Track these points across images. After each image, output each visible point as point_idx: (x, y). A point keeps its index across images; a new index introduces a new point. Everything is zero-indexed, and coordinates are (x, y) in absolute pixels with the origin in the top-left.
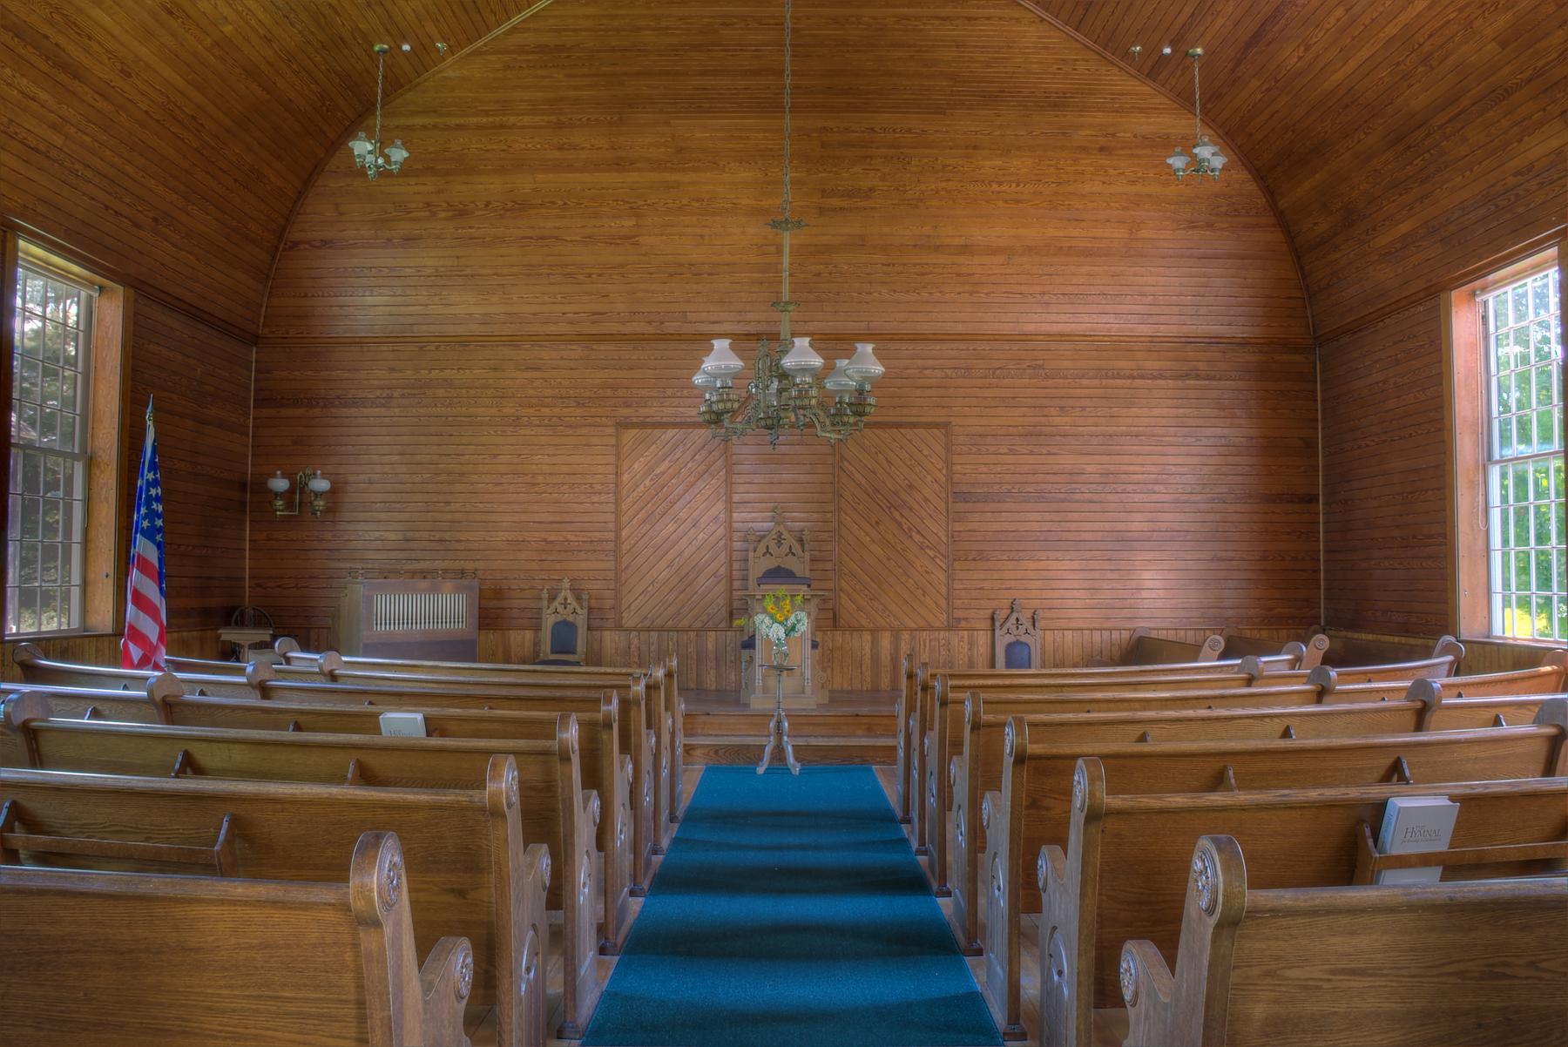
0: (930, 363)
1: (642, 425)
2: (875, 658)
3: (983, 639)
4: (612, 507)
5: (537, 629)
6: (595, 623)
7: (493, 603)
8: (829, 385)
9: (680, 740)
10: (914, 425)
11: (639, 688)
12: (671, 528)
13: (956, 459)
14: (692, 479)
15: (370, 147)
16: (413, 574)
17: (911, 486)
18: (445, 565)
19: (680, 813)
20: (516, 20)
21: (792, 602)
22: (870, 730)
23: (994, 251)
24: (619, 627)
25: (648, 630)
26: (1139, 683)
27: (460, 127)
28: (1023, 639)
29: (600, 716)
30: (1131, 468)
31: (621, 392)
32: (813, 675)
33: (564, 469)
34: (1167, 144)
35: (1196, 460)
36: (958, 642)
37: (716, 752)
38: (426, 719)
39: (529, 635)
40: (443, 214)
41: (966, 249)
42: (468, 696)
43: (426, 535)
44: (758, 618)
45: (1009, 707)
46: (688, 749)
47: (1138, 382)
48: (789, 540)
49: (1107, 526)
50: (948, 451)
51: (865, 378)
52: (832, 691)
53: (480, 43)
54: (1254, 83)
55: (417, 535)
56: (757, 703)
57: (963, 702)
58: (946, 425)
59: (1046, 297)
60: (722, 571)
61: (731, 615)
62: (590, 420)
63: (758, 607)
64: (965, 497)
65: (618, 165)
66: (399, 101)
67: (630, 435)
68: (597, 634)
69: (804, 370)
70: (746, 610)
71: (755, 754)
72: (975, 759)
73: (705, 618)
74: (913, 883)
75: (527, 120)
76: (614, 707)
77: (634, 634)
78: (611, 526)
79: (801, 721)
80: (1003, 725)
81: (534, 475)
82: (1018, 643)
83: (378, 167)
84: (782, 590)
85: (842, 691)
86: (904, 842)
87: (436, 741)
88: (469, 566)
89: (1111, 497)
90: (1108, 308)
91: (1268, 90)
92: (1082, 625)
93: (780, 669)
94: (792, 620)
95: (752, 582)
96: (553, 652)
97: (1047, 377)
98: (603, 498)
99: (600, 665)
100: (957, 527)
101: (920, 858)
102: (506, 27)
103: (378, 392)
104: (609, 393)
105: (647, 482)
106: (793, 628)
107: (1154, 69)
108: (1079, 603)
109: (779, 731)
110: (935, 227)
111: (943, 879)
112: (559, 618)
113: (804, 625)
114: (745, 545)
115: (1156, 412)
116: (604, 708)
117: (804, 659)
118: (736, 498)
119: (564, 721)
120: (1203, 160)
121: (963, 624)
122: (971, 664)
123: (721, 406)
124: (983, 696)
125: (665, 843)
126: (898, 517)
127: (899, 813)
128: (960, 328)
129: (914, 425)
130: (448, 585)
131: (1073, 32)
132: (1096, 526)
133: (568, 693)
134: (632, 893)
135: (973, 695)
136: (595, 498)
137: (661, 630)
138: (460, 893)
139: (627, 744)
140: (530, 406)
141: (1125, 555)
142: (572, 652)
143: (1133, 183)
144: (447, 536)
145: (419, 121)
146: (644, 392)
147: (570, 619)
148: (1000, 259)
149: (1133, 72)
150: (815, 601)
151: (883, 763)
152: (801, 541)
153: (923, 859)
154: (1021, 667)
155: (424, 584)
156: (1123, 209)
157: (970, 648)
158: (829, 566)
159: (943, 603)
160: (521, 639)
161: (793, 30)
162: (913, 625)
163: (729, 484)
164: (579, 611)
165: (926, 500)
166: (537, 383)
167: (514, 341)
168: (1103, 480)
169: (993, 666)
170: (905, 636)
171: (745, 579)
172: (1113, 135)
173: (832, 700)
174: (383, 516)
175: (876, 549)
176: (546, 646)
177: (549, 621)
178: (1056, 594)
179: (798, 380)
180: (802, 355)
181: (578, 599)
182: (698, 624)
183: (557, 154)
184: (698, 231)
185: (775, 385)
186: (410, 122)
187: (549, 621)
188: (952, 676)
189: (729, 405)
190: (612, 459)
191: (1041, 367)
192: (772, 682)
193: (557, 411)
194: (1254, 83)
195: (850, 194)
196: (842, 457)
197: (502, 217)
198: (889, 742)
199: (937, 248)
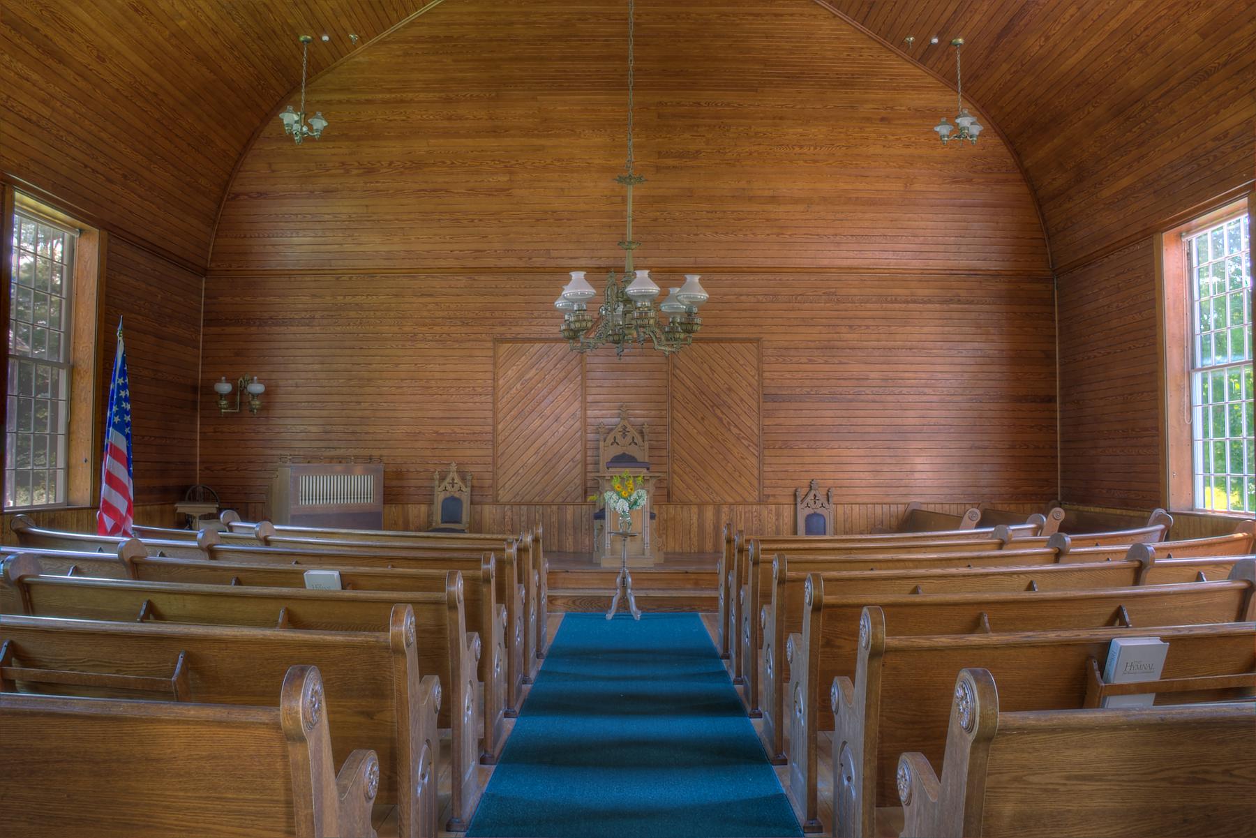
1: (514, 340)
2: (701, 527)
3: (787, 511)
5: (431, 503)
6: (477, 499)
7: (394, 483)
8: (664, 308)
9: (545, 592)
10: (732, 340)
11: (512, 551)
12: (537, 422)
13: (766, 367)
14: (554, 383)
15: (296, 118)
16: (331, 459)
17: (730, 389)
19: (545, 651)
20: (414, 16)
21: (634, 482)
22: (697, 584)
23: (796, 201)
24: (496, 502)
25: (520, 504)
27: (368, 102)
28: (819, 511)
30: (907, 375)
31: (497, 314)
32: (651, 540)
33: (452, 375)
34: (935, 115)
35: (958, 368)
36: (767, 514)
37: (574, 602)
38: (341, 575)
39: (423, 508)
40: (355, 172)
41: (773, 199)
42: (375, 557)
43: (341, 428)
44: (607, 495)
45: (807, 565)
46: (551, 599)
47: (911, 306)
48: (633, 432)
49: (887, 421)
52: (666, 554)
53: (384, 34)
55: (334, 428)
56: (607, 562)
57: (771, 562)
58: (758, 340)
60: (579, 457)
61: (586, 493)
62: (473, 337)
63: (607, 486)
64: (774, 398)
65: (495, 132)
66: (320, 81)
68: (478, 508)
69: (644, 296)
70: (598, 489)
71: (605, 603)
72: (781, 608)
74: (731, 707)
75: (422, 96)
76: (492, 566)
77: (507, 507)
78: (490, 421)
79: (641, 578)
80: (803, 580)
82: (815, 514)
83: (303, 134)
84: (626, 472)
86: (724, 674)
87: (349, 593)
88: (376, 453)
89: (890, 398)
93: (625, 535)
94: (634, 496)
95: (602, 466)
97: (838, 302)
98: (483, 398)
100: (767, 422)
102: (405, 21)
103: (303, 314)
104: (488, 314)
105: (518, 386)
106: (635, 503)
107: (924, 56)
110: (749, 182)
111: (755, 703)
112: (448, 495)
114: (597, 436)
115: (926, 330)
116: (484, 567)
117: (644, 527)
118: (590, 398)
119: (452, 577)
120: (964, 128)
121: (771, 499)
122: (778, 532)
123: (578, 325)
125: (533, 675)
127: (720, 651)
128: (769, 263)
129: (732, 340)
130: (359, 468)
131: (859, 26)
132: (878, 421)
134: (507, 715)
135: (779, 556)
136: (477, 399)
137: (529, 504)
138: (369, 715)
139: (502, 595)
141: (901, 444)
142: (458, 522)
143: (907, 146)
144: (358, 429)
146: (516, 314)
147: (457, 495)
148: (801, 208)
149: (907, 57)
150: (653, 481)
151: (707, 611)
152: (641, 433)
155: (339, 467)
156: (900, 167)
157: (776, 518)
158: (664, 453)
159: (756, 483)
160: (417, 511)
162: (731, 500)
163: (584, 387)
164: (464, 489)
165: (742, 400)
166: (430, 307)
167: (412, 273)
169: (795, 533)
170: (725, 509)
171: (597, 463)
172: (892, 108)
173: (667, 561)
174: (306, 413)
175: (702, 440)
176: (438, 518)
177: (440, 497)
178: (846, 475)
179: (639, 304)
180: (642, 284)
181: (463, 479)
182: (559, 500)
183: (446, 124)
185: (621, 308)
186: (328, 97)
187: (440, 497)
188: (763, 541)
189: (584, 324)
190: (490, 368)
191: (834, 294)
192: (618, 546)
193: (446, 329)
194: (1005, 67)
196: (675, 366)
197: (402, 173)
199: (751, 199)
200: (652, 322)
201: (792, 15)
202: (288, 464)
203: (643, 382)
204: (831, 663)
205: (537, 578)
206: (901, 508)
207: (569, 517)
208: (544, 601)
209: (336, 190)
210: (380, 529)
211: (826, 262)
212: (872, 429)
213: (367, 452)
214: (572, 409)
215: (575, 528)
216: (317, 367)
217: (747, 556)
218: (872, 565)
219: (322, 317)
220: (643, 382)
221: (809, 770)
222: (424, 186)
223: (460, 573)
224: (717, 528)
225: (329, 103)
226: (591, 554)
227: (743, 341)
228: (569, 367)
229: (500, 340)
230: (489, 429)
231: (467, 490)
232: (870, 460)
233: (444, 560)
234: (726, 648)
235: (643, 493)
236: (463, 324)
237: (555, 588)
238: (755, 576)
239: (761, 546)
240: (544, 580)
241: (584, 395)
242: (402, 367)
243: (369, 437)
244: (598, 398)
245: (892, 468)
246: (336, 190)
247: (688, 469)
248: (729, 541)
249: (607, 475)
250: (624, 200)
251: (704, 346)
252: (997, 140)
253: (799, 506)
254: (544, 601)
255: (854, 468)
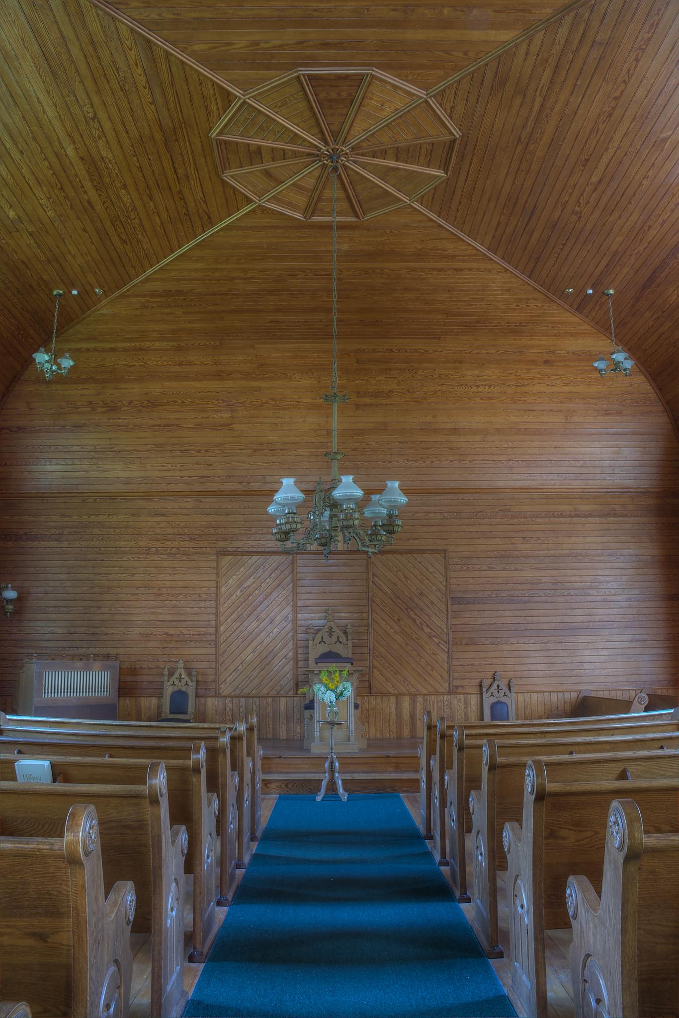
0: (433, 508)
1: (235, 553)
2: (399, 715)
3: (474, 700)
4: (213, 610)
5: (160, 696)
6: (201, 692)
7: (129, 678)
8: (367, 513)
9: (260, 777)
10: (422, 552)
11: (225, 740)
12: (255, 624)
13: (452, 574)
14: (269, 590)
15: (47, 358)
16: (73, 657)
17: (422, 594)
18: (96, 651)
19: (259, 834)
20: (149, 272)
21: (340, 675)
22: (397, 768)
23: (474, 432)
24: (218, 695)
25: (239, 697)
26: (602, 729)
27: (113, 350)
28: (503, 699)
29: (190, 763)
30: (573, 579)
31: (220, 531)
32: (356, 728)
33: (181, 584)
34: (590, 357)
35: (617, 572)
36: (457, 702)
37: (287, 785)
38: (53, 765)
39: (154, 701)
40: (100, 410)
41: (455, 431)
42: (94, 746)
43: (83, 630)
44: (316, 687)
45: (510, 750)
46: (266, 783)
47: (575, 519)
48: (338, 632)
49: (559, 619)
50: (446, 569)
51: (395, 506)
52: (369, 739)
53: (125, 289)
54: (648, 314)
55: (78, 630)
56: (316, 749)
57: (481, 747)
58: (445, 551)
59: (511, 463)
60: (291, 654)
61: (297, 686)
62: (199, 550)
63: (316, 680)
64: (456, 600)
65: (219, 376)
66: (71, 331)
67: (226, 560)
68: (203, 700)
69: (350, 499)
70: (307, 682)
71: (312, 786)
72: (492, 794)
73: (278, 688)
74: (438, 890)
75: (157, 344)
76: (202, 756)
77: (228, 700)
78: (213, 623)
79: (347, 762)
80: (524, 765)
81: (160, 588)
82: (499, 702)
83: (53, 371)
84: (333, 667)
85: (376, 739)
86: (428, 855)
87: (60, 787)
88: (113, 651)
89: (560, 599)
90: (553, 470)
91: (658, 318)
92: (543, 688)
93: (332, 724)
94: (341, 688)
95: (311, 662)
96: (171, 713)
97: (513, 517)
98: (207, 604)
99: (204, 721)
100: (455, 621)
101: (442, 868)
102: (142, 277)
103: (53, 531)
104: (212, 531)
105: (238, 593)
106: (341, 694)
107: (581, 305)
108: (541, 674)
109: (332, 770)
110: (434, 416)
111: (464, 887)
112: (176, 689)
113: (349, 692)
114: (307, 636)
115: (588, 540)
116: (193, 756)
117: (350, 717)
118: (300, 603)
119: (154, 767)
120: (619, 362)
121: (460, 690)
122: (466, 717)
123: (288, 527)
124: (498, 742)
125: (247, 859)
126: (414, 616)
127: (422, 829)
128: (453, 485)
129: (422, 552)
130: (97, 665)
131: (526, 279)
132: (550, 619)
133: (170, 743)
134: (219, 904)
135: (489, 741)
136: (202, 604)
137: (247, 697)
138: (42, 937)
139: (214, 784)
140: (157, 540)
141: (572, 639)
142: (185, 713)
143: (567, 384)
144: (98, 630)
145: (84, 345)
146: (236, 531)
147: (184, 689)
148: (478, 438)
149: (567, 307)
150: (357, 675)
151: (407, 792)
152: (345, 633)
153: (445, 869)
154: (502, 720)
155: (79, 664)
156: (561, 403)
157: (463, 708)
158: (365, 650)
159: (446, 675)
160: (149, 703)
161: (339, 279)
162: (425, 692)
163: (294, 593)
164: (190, 684)
165: (432, 603)
166: (163, 524)
167: (147, 496)
168: (554, 587)
169: (482, 719)
170: (420, 699)
171: (307, 660)
172: (553, 352)
173: (369, 746)
174: (53, 616)
175: (399, 638)
176: (166, 708)
177: (169, 690)
178: (525, 668)
179: (345, 507)
180: (348, 488)
181: (189, 675)
182: (274, 693)
183: (177, 368)
184: (273, 420)
185: (327, 513)
186: (78, 346)
187: (169, 690)
188: (467, 727)
189: (294, 526)
190: (214, 577)
191: (509, 510)
192: (327, 733)
193: (176, 543)
194: (648, 314)
195: (377, 394)
196: (374, 575)
197: (140, 411)
198: (412, 776)
199: (436, 431)
200: (356, 522)
201: (470, 269)
202: (34, 660)
203: (346, 589)
204: (567, 859)
205: (251, 765)
206: (574, 695)
207: (282, 708)
208: (259, 786)
209: (84, 425)
210: (114, 719)
211: (501, 484)
212: (546, 626)
213: (105, 651)
214: (284, 613)
215: (288, 718)
216: (64, 576)
217: (450, 744)
218: (571, 749)
219: (70, 533)
220: (346, 589)
221: (537, 977)
222: (158, 422)
223: (163, 764)
224: (413, 716)
225: (79, 350)
226: (302, 740)
227: (432, 552)
228: (283, 576)
229: (223, 553)
230: (212, 630)
231: (192, 685)
232: (544, 653)
233: (159, 748)
234: (429, 828)
235: (348, 684)
236: (191, 539)
237: (269, 773)
238: (460, 762)
239: (465, 732)
240: (259, 763)
241: (295, 601)
242: (137, 577)
243: (105, 637)
244: (308, 602)
245: (565, 660)
246: (84, 425)
247: (386, 665)
248: (430, 727)
249: (316, 670)
250: (329, 433)
251: (398, 556)
252: (642, 378)
253: (485, 695)
254: (259, 786)
255: (531, 660)
